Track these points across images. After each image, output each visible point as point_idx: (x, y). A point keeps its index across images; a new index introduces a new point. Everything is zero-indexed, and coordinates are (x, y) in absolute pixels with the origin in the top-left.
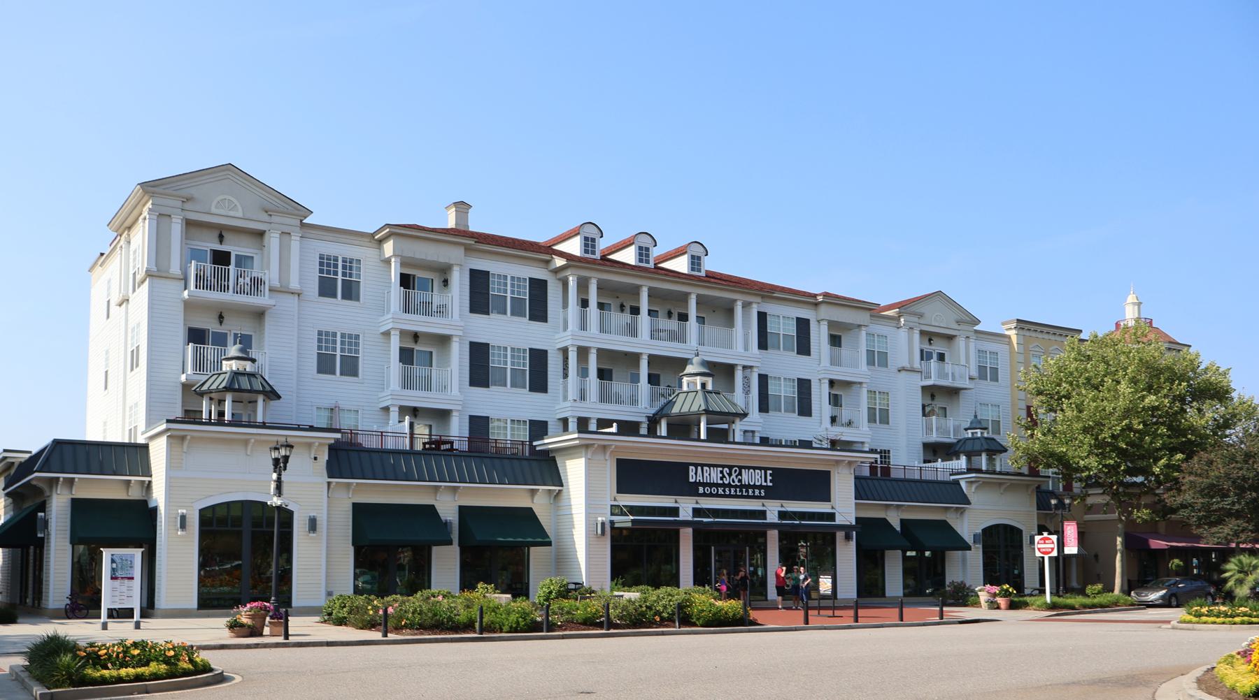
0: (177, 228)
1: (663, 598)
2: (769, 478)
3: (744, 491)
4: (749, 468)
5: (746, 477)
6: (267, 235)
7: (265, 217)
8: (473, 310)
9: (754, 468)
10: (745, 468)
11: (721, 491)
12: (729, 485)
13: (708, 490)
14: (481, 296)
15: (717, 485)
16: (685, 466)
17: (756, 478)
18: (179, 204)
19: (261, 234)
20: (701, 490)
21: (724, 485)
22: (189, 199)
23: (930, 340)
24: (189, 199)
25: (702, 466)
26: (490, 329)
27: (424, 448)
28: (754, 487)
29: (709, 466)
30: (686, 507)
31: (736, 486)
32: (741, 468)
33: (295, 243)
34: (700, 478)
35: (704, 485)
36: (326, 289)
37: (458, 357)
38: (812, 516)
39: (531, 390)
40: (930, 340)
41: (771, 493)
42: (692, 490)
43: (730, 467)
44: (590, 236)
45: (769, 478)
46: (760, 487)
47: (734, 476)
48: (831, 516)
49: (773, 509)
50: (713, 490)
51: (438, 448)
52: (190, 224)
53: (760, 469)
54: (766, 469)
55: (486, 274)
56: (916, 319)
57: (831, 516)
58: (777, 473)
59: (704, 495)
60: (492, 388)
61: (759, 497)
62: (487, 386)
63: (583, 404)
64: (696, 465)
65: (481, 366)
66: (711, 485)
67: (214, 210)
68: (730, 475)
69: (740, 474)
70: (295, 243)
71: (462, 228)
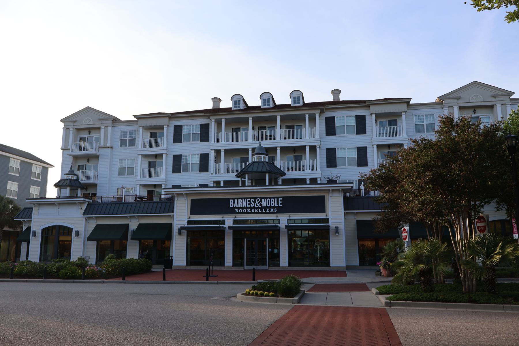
0: (71, 132)
1: (241, 268)
2: (280, 202)
3: (263, 210)
4: (267, 198)
5: (264, 203)
6: (495, 106)
7: (493, 99)
8: (327, 134)
9: (270, 198)
10: (264, 198)
11: (249, 211)
12: (254, 207)
13: (241, 211)
14: (178, 136)
15: (247, 208)
16: (228, 200)
17: (272, 203)
18: (72, 124)
19: (492, 107)
20: (237, 211)
21: (251, 208)
22: (75, 122)
23: (474, 111)
24: (75, 122)
25: (238, 199)
26: (179, 149)
27: (136, 200)
28: (270, 207)
29: (242, 199)
30: (229, 220)
31: (258, 208)
32: (261, 198)
33: (110, 129)
34: (236, 205)
35: (238, 208)
36: (123, 143)
37: (321, 156)
38: (245, 221)
39: (358, 166)
40: (474, 111)
41: (280, 210)
42: (232, 211)
43: (255, 199)
44: (237, 100)
45: (280, 202)
46: (274, 207)
47: (257, 202)
48: (327, 220)
49: (283, 220)
50: (243, 210)
51: (142, 200)
52: (461, 108)
53: (274, 198)
54: (278, 198)
55: (333, 118)
56: (455, 101)
57: (327, 220)
58: (284, 199)
59: (239, 213)
60: (182, 173)
61: (274, 213)
62: (336, 167)
63: (217, 175)
64: (234, 199)
65: (178, 165)
66: (243, 208)
67: (84, 124)
68: (255, 202)
69: (261, 201)
70: (110, 129)
71: (337, 100)
